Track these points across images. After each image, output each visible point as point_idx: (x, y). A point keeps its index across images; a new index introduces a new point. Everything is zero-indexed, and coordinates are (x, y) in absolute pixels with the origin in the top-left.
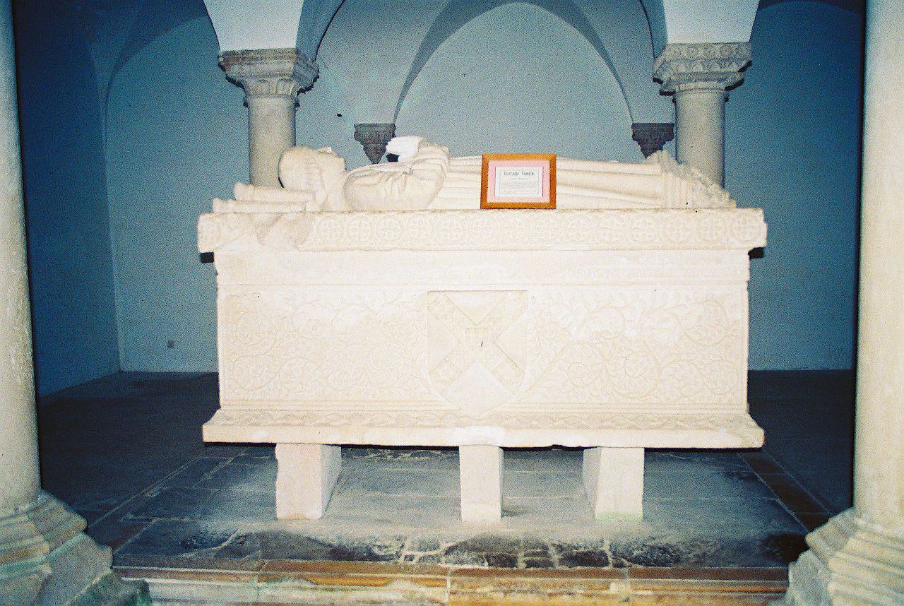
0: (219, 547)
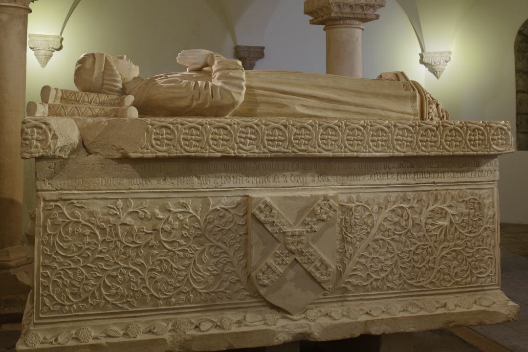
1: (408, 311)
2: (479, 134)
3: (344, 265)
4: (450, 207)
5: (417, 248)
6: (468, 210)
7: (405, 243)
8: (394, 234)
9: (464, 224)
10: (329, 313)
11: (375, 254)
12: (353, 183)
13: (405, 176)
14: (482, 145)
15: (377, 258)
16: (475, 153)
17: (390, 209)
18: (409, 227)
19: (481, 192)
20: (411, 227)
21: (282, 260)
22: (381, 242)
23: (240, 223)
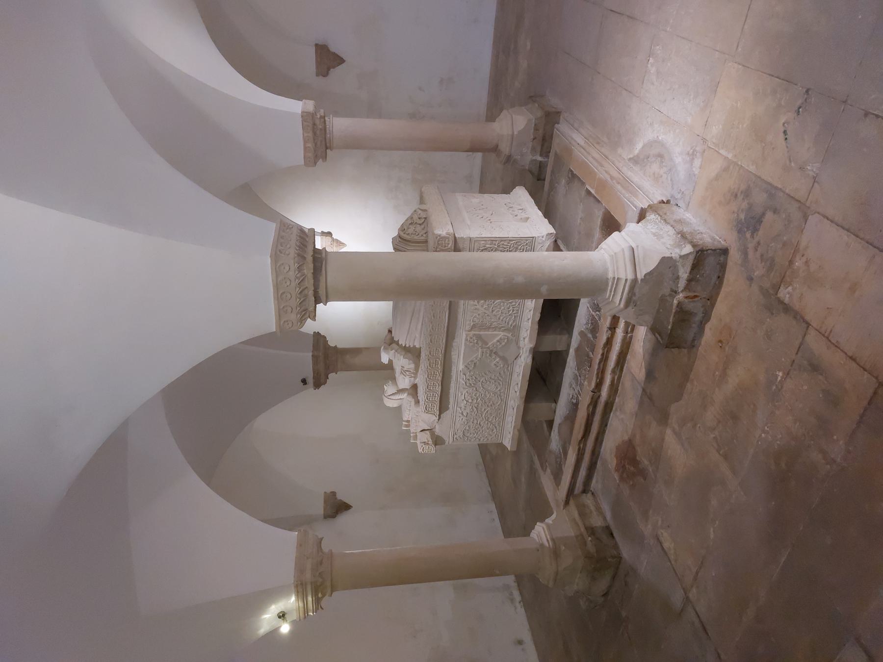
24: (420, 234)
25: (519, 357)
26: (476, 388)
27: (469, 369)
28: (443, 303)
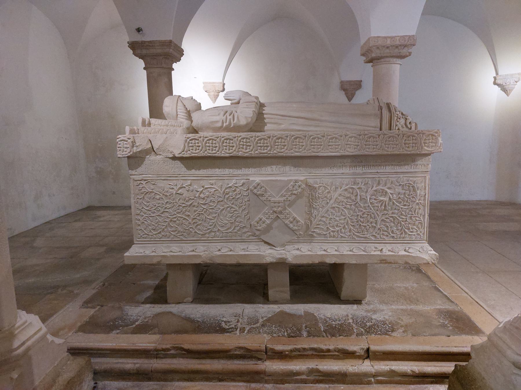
0: (134, 326)
1: (353, 251)
2: (413, 139)
3: (311, 221)
4: (389, 188)
5: (363, 214)
6: (404, 191)
7: (354, 210)
8: (346, 204)
9: (400, 200)
10: (300, 248)
11: (332, 215)
12: (317, 172)
13: (356, 168)
14: (415, 146)
15: (334, 218)
16: (409, 152)
17: (344, 189)
18: (357, 200)
19: (415, 179)
20: (359, 201)
21: (269, 216)
22: (337, 209)
23: (245, 195)
24: (398, 123)
25: (269, 247)
26: (222, 201)
27: (255, 188)
28: (350, 148)
